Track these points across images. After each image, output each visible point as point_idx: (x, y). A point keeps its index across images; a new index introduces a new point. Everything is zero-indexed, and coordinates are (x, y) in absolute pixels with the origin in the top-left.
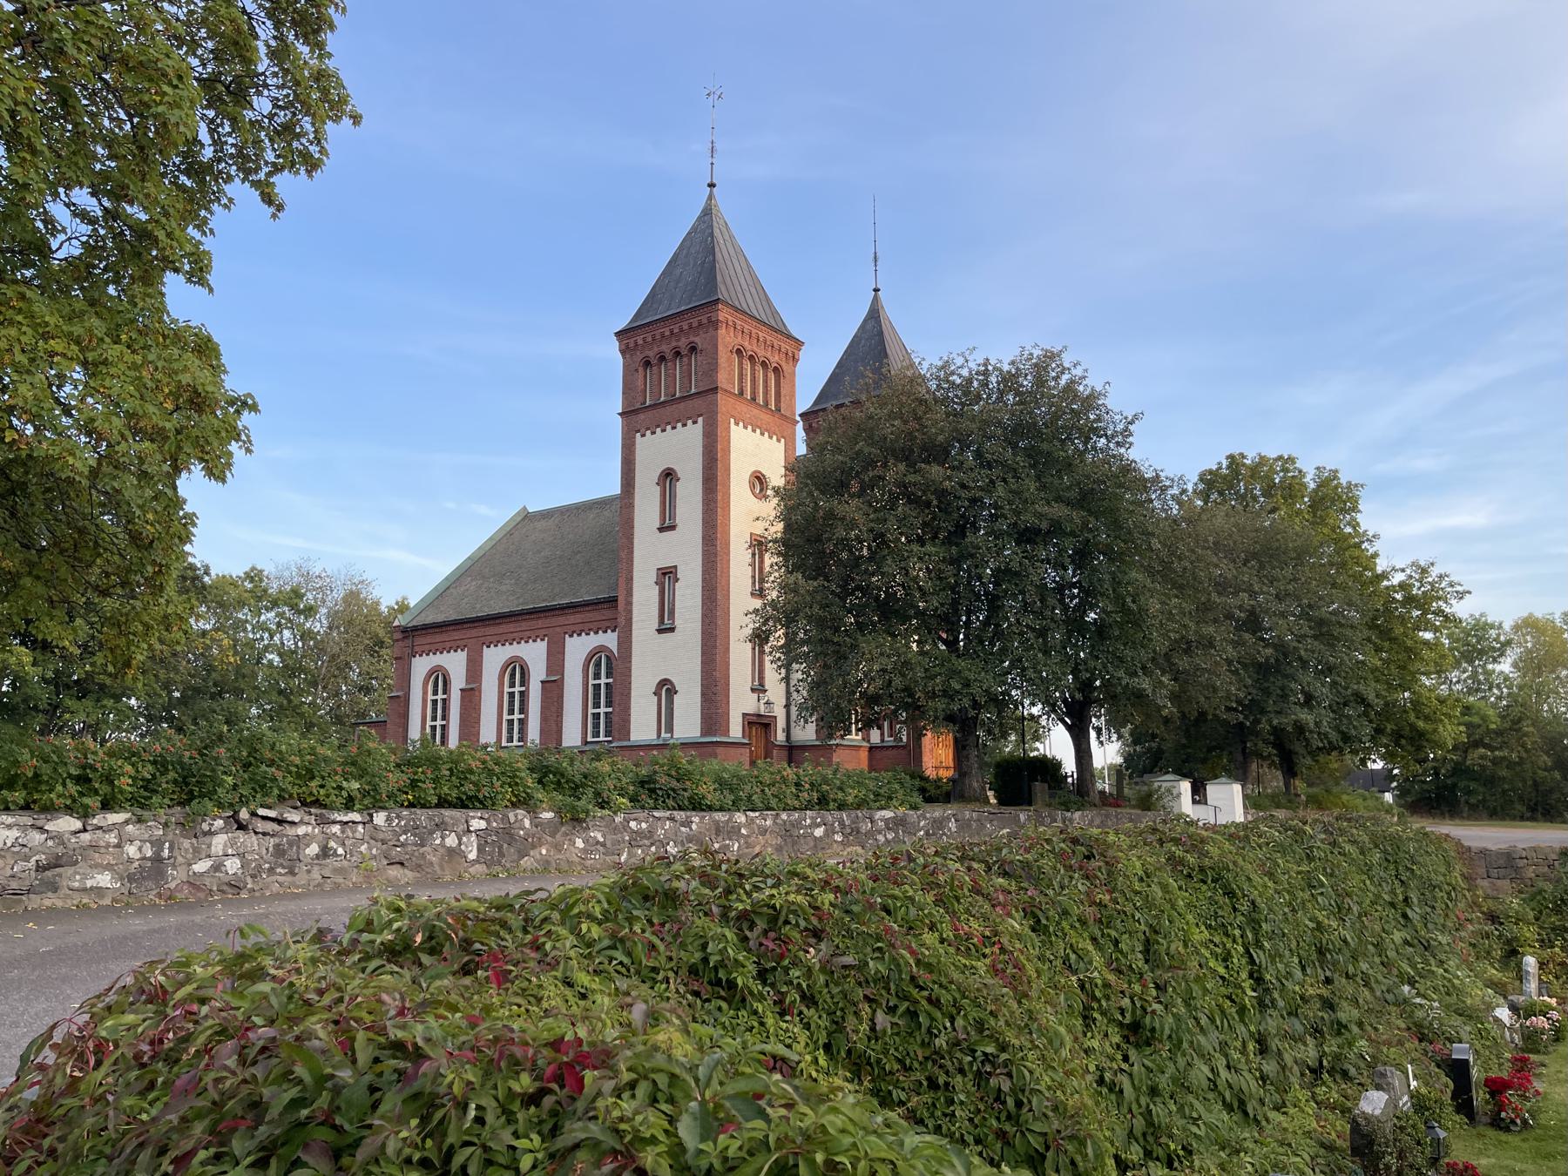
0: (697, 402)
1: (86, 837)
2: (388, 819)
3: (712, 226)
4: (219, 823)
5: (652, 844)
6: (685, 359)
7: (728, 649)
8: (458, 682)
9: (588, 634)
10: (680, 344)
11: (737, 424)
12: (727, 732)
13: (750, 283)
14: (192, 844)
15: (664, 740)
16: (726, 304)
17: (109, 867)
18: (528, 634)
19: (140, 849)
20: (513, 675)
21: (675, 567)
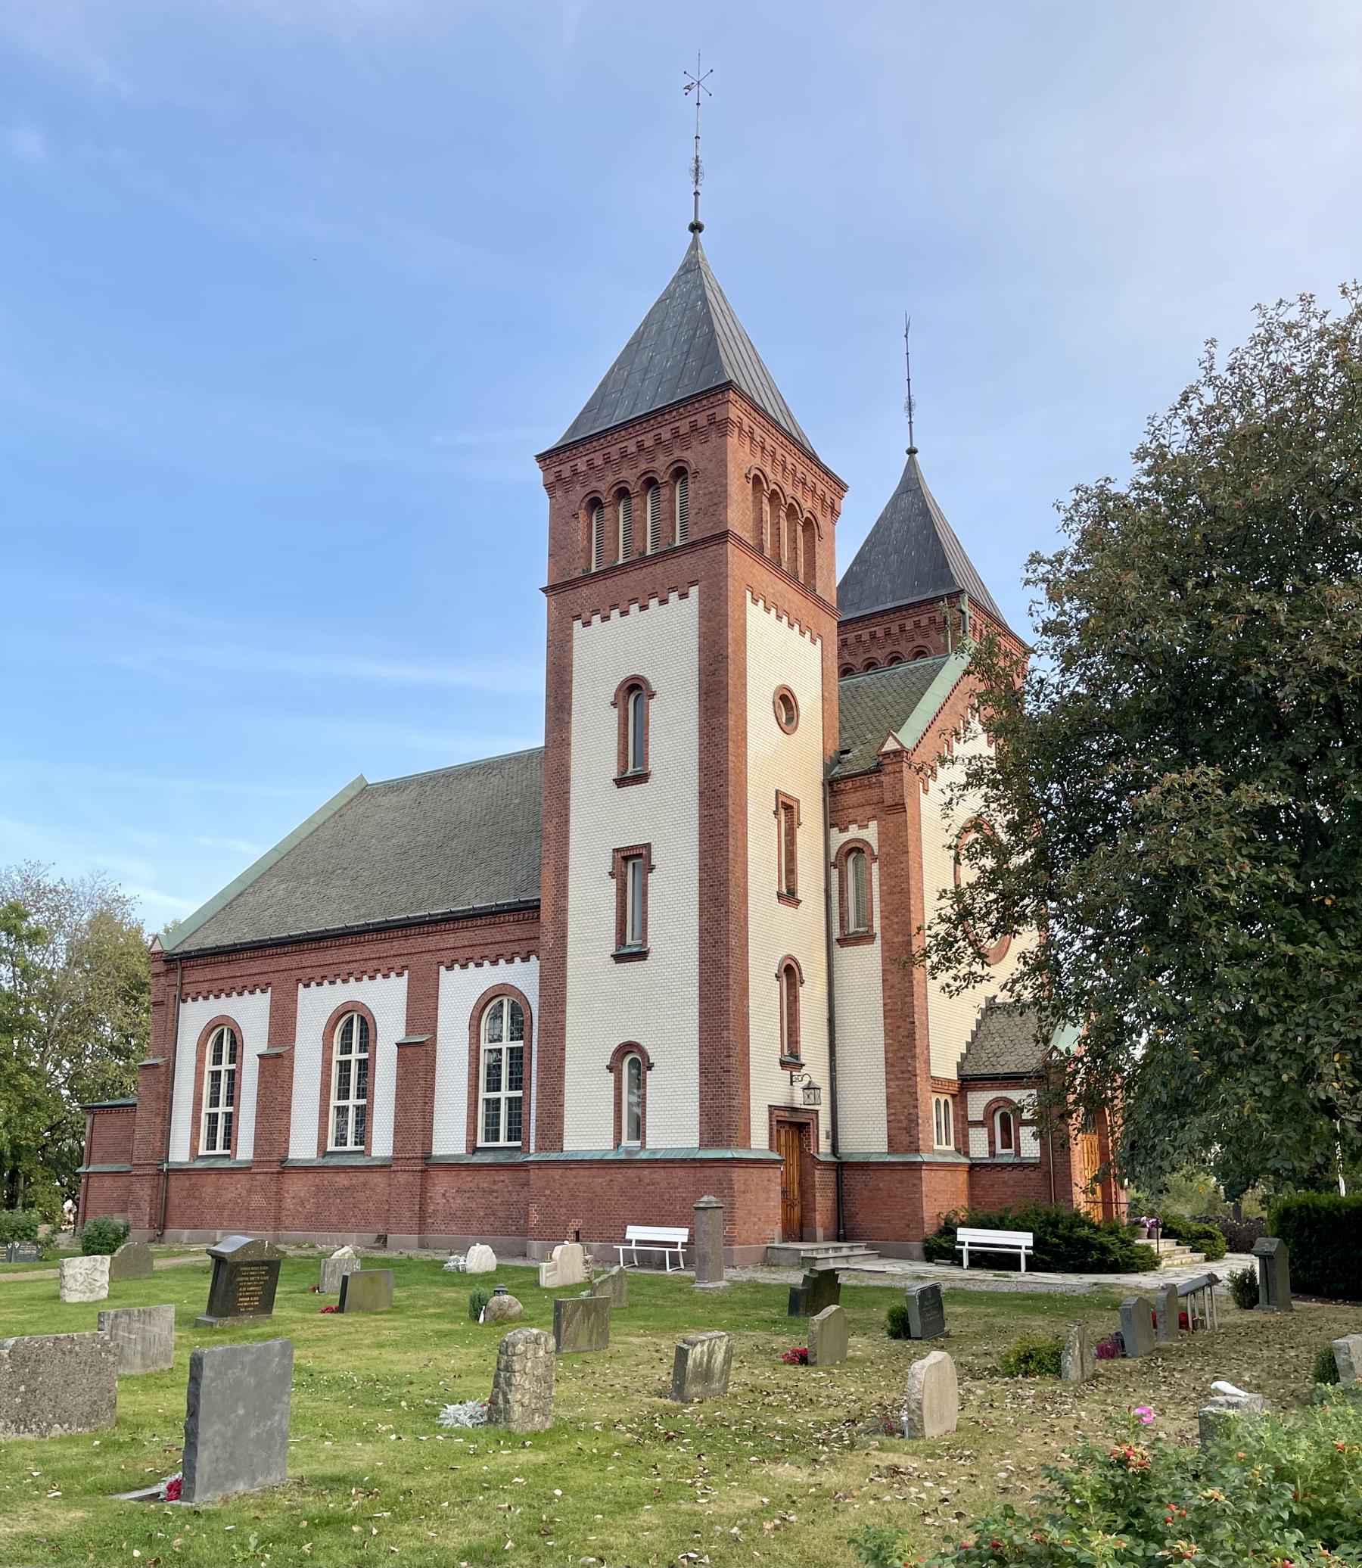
0: (687, 561)
3: (702, 285)
6: (665, 492)
7: (746, 990)
8: (255, 1043)
9: (479, 965)
10: (655, 465)
11: (755, 601)
12: (745, 1142)
13: (765, 383)
15: (628, 1152)
16: (743, 395)
18: (375, 964)
20: (347, 1033)
21: (648, 846)
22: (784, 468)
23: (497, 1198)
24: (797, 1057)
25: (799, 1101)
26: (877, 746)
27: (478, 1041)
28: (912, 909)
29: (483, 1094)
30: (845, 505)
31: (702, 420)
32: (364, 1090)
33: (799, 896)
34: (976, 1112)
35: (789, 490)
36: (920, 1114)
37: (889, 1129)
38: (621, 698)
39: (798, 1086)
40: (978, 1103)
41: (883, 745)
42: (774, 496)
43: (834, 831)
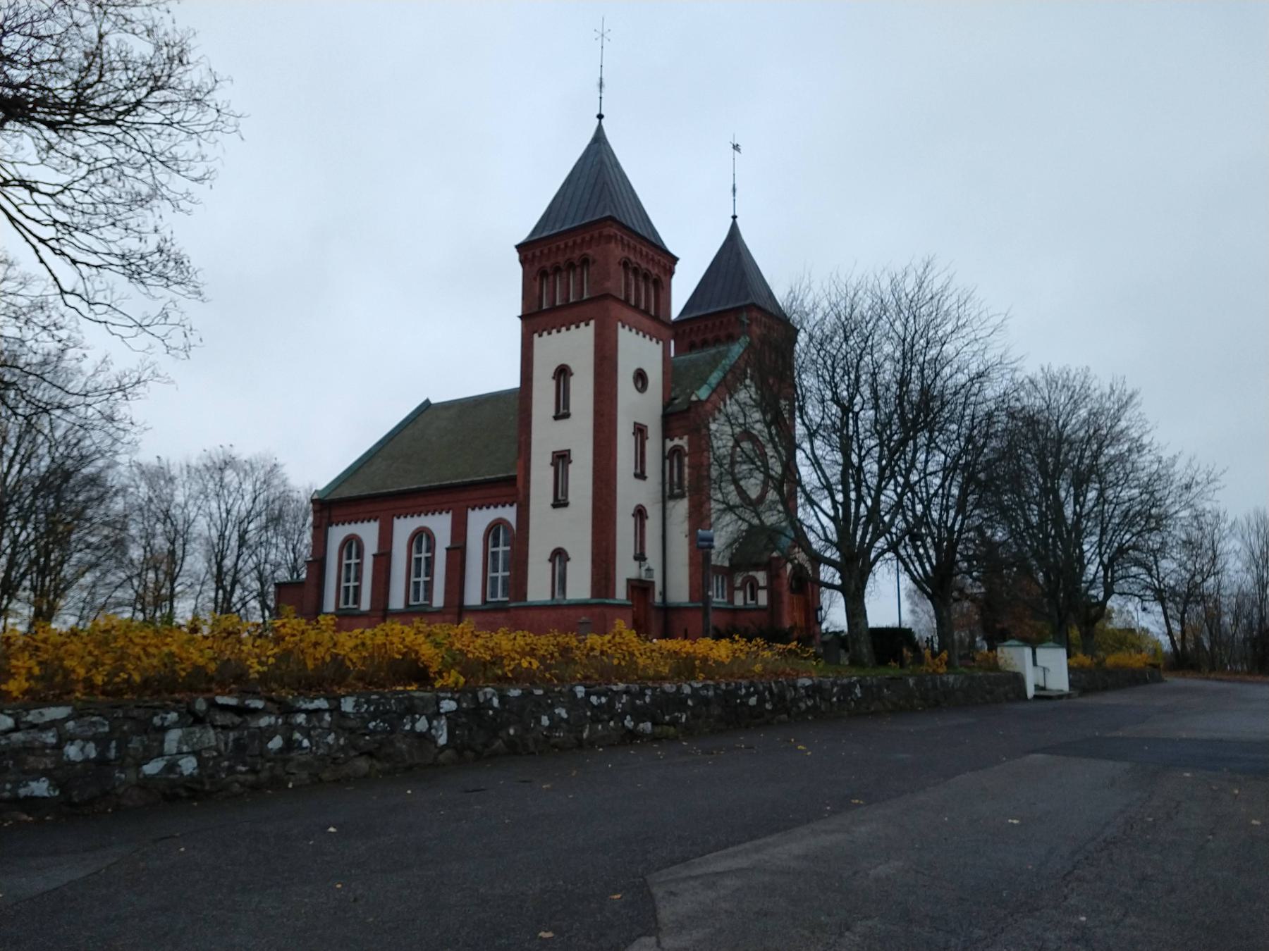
1: (18, 737)
2: (357, 705)
4: (173, 716)
5: (611, 719)
12: (613, 596)
14: (142, 742)
17: (46, 773)
19: (82, 749)
25: (643, 576)
31: (596, 234)
33: (647, 474)
34: (738, 581)
35: (644, 265)
39: (643, 569)
43: (668, 441)
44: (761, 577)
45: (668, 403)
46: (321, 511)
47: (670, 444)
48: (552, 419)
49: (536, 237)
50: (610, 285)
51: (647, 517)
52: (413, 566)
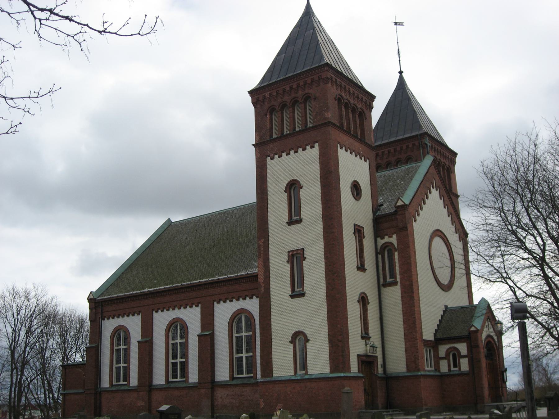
11: (341, 148)
12: (348, 370)
22: (350, 93)
23: (244, 398)
24: (368, 334)
26: (394, 203)
27: (232, 333)
28: (412, 270)
29: (171, 361)
30: (375, 103)
31: (316, 77)
32: (184, 354)
33: (366, 267)
34: (442, 353)
35: (352, 101)
36: (419, 355)
37: (407, 362)
38: (288, 189)
40: (443, 350)
41: (396, 203)
42: (346, 104)
43: (379, 239)
44: (463, 348)
45: (376, 207)
46: (95, 308)
47: (381, 242)
48: (287, 225)
49: (262, 85)
50: (329, 115)
51: (369, 303)
52: (116, 356)
